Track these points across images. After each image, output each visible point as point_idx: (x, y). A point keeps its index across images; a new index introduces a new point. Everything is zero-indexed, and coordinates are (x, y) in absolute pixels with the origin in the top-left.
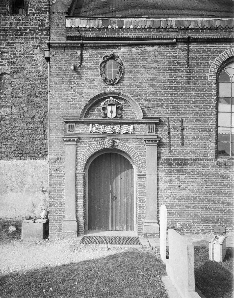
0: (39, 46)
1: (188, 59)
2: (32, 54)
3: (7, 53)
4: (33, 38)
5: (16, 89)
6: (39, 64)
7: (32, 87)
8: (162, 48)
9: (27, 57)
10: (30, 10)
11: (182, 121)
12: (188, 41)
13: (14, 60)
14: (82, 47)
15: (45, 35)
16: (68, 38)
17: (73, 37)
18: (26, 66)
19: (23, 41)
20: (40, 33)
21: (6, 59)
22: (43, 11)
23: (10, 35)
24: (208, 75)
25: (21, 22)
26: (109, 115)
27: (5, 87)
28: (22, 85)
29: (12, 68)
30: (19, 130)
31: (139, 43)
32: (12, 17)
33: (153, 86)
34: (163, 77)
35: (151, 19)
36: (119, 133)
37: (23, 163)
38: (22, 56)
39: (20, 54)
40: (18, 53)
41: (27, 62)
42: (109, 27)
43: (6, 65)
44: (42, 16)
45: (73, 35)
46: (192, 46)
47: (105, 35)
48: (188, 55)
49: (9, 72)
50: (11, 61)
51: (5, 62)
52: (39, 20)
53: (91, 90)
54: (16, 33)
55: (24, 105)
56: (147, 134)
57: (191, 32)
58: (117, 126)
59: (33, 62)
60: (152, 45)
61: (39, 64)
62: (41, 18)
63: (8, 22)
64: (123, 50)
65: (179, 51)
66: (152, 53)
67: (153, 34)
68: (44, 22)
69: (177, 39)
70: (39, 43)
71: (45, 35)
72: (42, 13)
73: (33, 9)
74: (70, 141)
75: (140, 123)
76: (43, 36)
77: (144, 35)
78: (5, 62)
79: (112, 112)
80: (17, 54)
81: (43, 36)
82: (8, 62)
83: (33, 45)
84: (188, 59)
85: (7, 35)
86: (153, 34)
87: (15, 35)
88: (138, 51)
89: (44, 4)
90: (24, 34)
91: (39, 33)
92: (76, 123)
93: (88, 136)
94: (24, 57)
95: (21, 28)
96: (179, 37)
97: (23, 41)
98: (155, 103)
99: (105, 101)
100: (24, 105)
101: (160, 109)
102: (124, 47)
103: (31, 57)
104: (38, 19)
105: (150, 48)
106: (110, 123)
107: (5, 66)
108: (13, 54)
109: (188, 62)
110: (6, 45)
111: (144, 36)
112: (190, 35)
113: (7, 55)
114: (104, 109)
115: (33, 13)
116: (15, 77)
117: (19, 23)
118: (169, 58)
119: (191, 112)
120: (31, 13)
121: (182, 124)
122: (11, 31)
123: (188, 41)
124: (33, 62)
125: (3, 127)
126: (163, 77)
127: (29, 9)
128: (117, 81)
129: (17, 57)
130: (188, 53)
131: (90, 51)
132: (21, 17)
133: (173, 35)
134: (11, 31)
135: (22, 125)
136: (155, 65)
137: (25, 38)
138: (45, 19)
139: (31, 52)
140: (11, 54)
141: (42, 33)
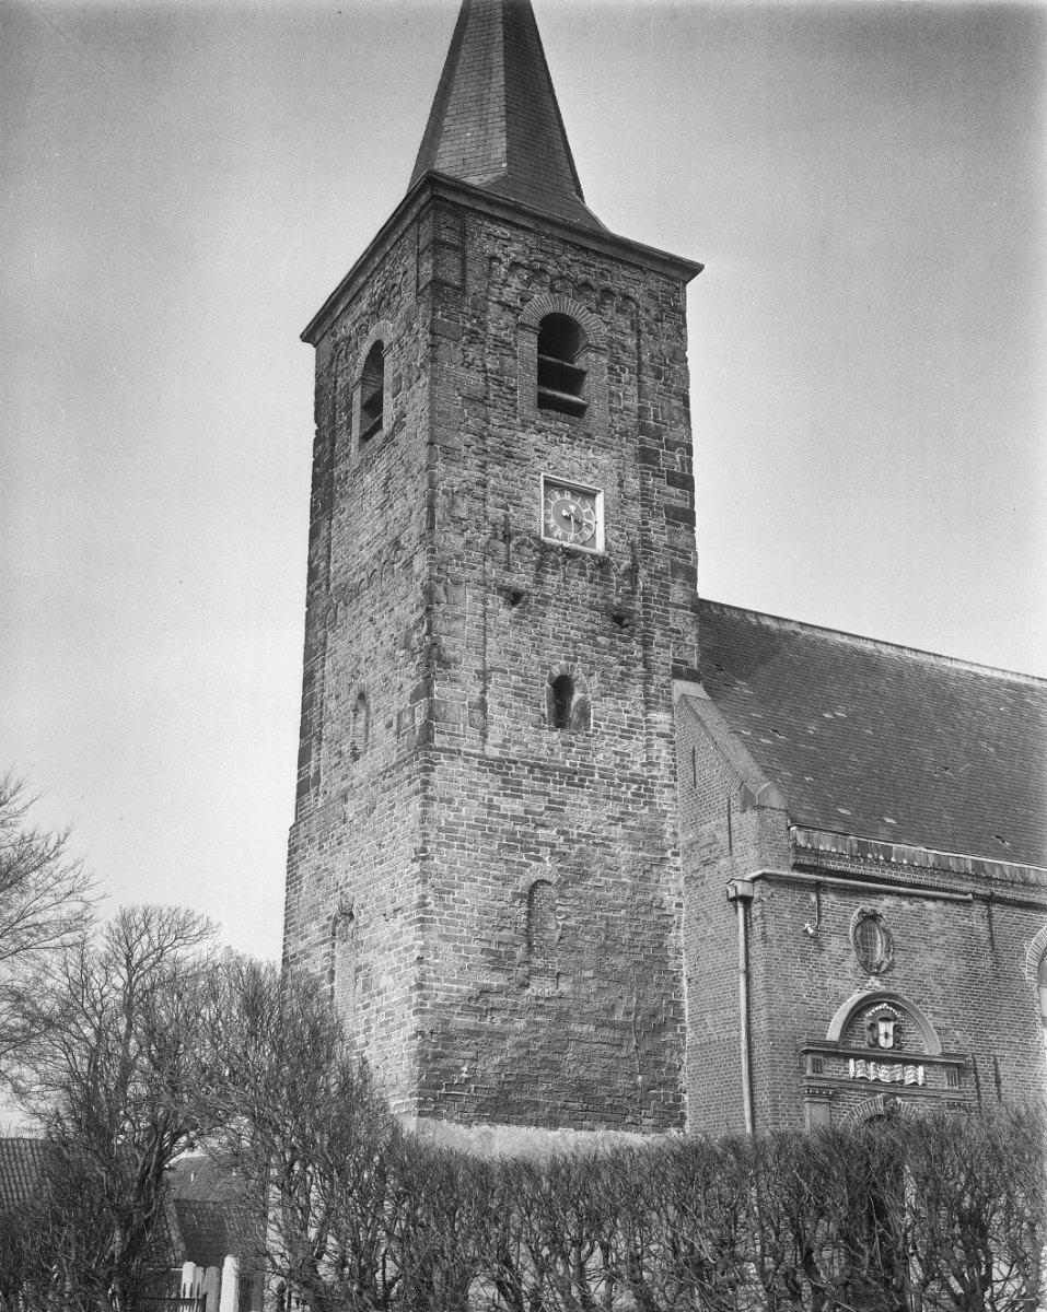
0: (623, 820)
1: (992, 934)
2: (607, 838)
3: (547, 827)
4: (608, 797)
5: (571, 928)
6: (623, 868)
7: (607, 925)
8: (949, 907)
9: (594, 844)
10: (595, 725)
11: (995, 1063)
12: (989, 900)
13: (564, 849)
14: (818, 887)
15: (634, 794)
16: (797, 867)
17: (806, 865)
18: (593, 868)
19: (585, 803)
20: (624, 789)
21: (547, 844)
22: (623, 731)
23: (555, 782)
24: (1025, 971)
25: (574, 750)
26: (882, 1042)
27: (541, 919)
28: (586, 918)
29: (560, 870)
30: (579, 1041)
31: (915, 891)
32: (555, 733)
33: (942, 984)
34: (955, 968)
35: (934, 852)
36: (902, 1081)
37: (590, 1141)
38: (584, 840)
39: (579, 835)
40: (576, 832)
41: (595, 859)
42: (870, 856)
43: (547, 858)
44: (620, 743)
45: (807, 862)
46: (995, 908)
47: (861, 871)
48: (991, 927)
49: (554, 879)
50: (558, 850)
51: (545, 852)
52: (616, 753)
53: (841, 982)
54: (569, 778)
55: (589, 974)
56: (946, 1087)
57: (996, 886)
58: (896, 1066)
59: (609, 860)
60: (934, 899)
61: (623, 868)
62: (619, 748)
63: (544, 744)
64: (888, 901)
65: (975, 917)
66: (934, 914)
67: (937, 880)
68: (627, 759)
69: (974, 894)
70: (622, 813)
71: (634, 794)
72: (620, 736)
73: (602, 724)
74: (820, 1095)
75: (934, 1063)
76: (629, 795)
77: (923, 879)
78: (545, 852)
79: (887, 1035)
80: (573, 834)
81: (629, 795)
82: (552, 854)
83: (609, 817)
84: (992, 934)
85: (548, 781)
86: (937, 880)
87: (568, 784)
88: (913, 908)
89: (626, 715)
90: (588, 783)
91: (620, 786)
92: (827, 1054)
93: (849, 1085)
94: (588, 844)
95: (575, 765)
96: (979, 891)
97: (585, 803)
98: (949, 1021)
99: (873, 1011)
100: (589, 974)
101: (957, 1033)
102: (889, 897)
103: (605, 846)
104: (613, 748)
105: (930, 905)
106: (880, 1061)
107: (545, 862)
108: (565, 833)
109: (992, 939)
110: (547, 808)
111: (923, 881)
112: (994, 889)
113: (549, 832)
114: (873, 1027)
115: (602, 733)
116: (568, 893)
117: (570, 751)
118: (962, 930)
119: (1006, 1045)
120: (596, 731)
121: (996, 1069)
122: (557, 773)
123: (989, 900)
124: (609, 860)
125: (542, 1031)
126: (955, 968)
127: (592, 721)
128: (884, 967)
129: (573, 841)
130: (990, 923)
131: (832, 897)
132: (573, 737)
133: (968, 886)
134: (557, 773)
135: (585, 1028)
136: (941, 941)
137: (591, 795)
138: (627, 751)
139: (604, 834)
140: (558, 832)
141: (628, 788)
